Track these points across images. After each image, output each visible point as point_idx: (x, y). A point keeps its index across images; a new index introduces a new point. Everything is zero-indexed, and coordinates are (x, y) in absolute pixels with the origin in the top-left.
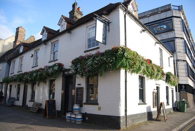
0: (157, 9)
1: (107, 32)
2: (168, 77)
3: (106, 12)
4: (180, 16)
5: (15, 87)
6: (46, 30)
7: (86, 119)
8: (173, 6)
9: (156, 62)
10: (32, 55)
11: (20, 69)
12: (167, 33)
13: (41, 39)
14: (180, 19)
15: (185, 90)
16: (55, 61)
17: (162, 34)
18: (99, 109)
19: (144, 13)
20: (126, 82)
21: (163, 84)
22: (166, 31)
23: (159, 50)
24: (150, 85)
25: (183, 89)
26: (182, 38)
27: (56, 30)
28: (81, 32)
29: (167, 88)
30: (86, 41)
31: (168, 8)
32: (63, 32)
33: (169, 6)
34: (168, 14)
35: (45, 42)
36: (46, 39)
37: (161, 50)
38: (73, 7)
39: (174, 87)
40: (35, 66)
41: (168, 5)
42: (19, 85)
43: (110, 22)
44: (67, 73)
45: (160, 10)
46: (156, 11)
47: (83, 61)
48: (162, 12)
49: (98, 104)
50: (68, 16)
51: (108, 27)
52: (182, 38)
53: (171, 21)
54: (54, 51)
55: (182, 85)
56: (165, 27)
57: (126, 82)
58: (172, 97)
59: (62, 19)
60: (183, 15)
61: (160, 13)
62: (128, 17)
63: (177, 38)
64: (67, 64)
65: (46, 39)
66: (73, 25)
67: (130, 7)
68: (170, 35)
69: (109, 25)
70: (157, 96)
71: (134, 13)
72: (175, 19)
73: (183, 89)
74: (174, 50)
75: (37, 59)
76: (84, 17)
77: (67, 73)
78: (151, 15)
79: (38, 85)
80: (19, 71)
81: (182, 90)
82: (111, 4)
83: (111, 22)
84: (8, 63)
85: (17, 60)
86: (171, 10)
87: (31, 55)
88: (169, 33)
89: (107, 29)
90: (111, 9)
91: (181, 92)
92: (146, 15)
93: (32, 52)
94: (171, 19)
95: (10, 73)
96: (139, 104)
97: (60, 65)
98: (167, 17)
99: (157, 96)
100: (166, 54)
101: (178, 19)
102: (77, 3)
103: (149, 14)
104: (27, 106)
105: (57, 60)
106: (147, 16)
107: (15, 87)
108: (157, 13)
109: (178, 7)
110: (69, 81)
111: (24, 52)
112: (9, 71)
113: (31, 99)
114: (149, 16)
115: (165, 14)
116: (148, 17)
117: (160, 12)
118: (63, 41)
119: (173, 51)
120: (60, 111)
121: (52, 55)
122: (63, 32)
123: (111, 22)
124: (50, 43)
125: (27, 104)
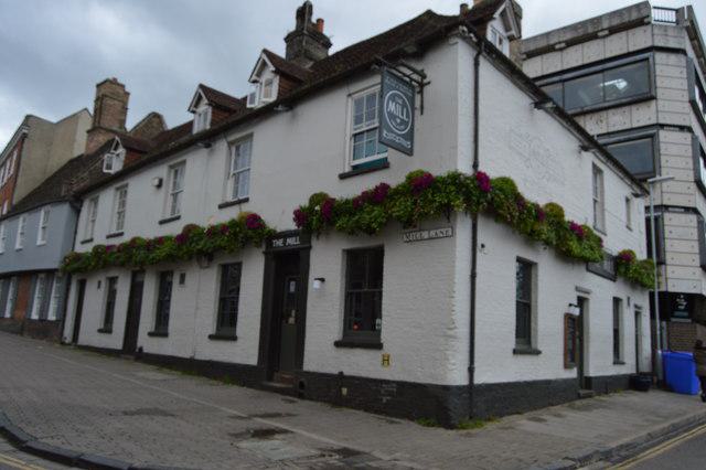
0: (596, 20)
1: (417, 113)
2: (622, 267)
3: (415, 50)
4: (682, 47)
5: (99, 287)
6: (207, 94)
7: (341, 394)
8: (655, 8)
9: (577, 212)
10: (161, 181)
11: (115, 225)
12: (626, 109)
13: (190, 124)
14: (682, 58)
15: (686, 314)
16: (240, 202)
17: (611, 112)
18: (386, 360)
19: (548, 35)
20: (473, 276)
21: (602, 291)
22: (624, 101)
23: (589, 172)
24: (556, 287)
25: (680, 310)
26: (682, 128)
27: (239, 95)
28: (332, 117)
29: (617, 301)
30: (345, 148)
31: (634, 16)
32: (267, 112)
33: (639, 11)
34: (638, 39)
35: (208, 139)
36: (208, 127)
37: (597, 171)
38: (297, 18)
39: (645, 303)
40: (168, 216)
41: (637, 6)
42: (113, 281)
43: (425, 81)
44: (279, 243)
45: (606, 25)
46: (590, 30)
47: (405, 219)
48: (613, 31)
49: (379, 346)
50: (280, 50)
51: (418, 97)
52: (682, 128)
53: (646, 63)
54: (235, 168)
55: (676, 295)
56: (622, 84)
57: (473, 276)
58: (637, 336)
59: (264, 64)
60: (691, 40)
61: (607, 36)
62: (486, 68)
63: (662, 126)
64: (280, 218)
65: (208, 127)
66: (299, 82)
67: (494, 31)
68: (641, 116)
69: (421, 92)
70: (575, 328)
71: (505, 50)
72: (660, 57)
73: (680, 310)
74: (650, 168)
75: (175, 195)
76: (337, 55)
77: (279, 243)
78: (570, 43)
79: (182, 280)
80: (114, 231)
81: (677, 313)
82: (429, 13)
83: (429, 83)
84: (72, 206)
85: (108, 198)
86: (649, 23)
87: (156, 182)
88: (634, 108)
89: (418, 104)
90: (426, 34)
91: (674, 320)
92: (552, 42)
93: (162, 171)
94: (646, 55)
95: (80, 237)
96: (515, 352)
97: (254, 221)
98: (631, 49)
99: (575, 328)
100: (615, 187)
101: (673, 58)
102: (311, 7)
103: (565, 39)
104: (141, 349)
105: (246, 200)
106: (557, 47)
107: (99, 287)
108: (593, 37)
109: (677, 11)
110: (288, 269)
111: (129, 171)
112: (76, 232)
113: (156, 328)
114: (563, 45)
115: (624, 38)
116: (561, 49)
117: (607, 32)
118: (267, 139)
119: (640, 181)
120: (253, 367)
121: (231, 184)
122: (267, 112)
123: (429, 83)
124: (222, 147)
125: (139, 345)
